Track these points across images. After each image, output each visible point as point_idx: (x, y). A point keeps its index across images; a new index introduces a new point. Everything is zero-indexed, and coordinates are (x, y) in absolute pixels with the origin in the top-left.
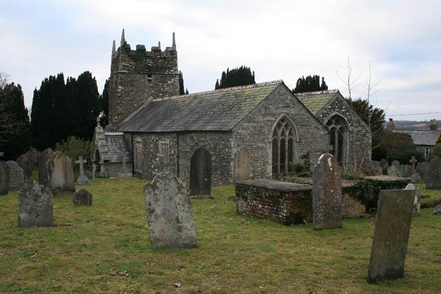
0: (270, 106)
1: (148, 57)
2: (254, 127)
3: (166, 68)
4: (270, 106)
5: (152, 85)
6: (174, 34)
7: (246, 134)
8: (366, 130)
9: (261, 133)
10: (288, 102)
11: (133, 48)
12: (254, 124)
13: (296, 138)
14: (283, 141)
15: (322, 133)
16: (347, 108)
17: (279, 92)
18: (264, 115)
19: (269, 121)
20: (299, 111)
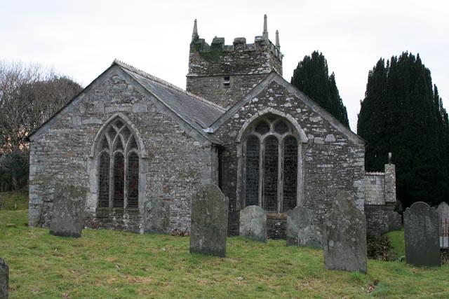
0: (95, 103)
1: (225, 53)
2: (67, 135)
3: (250, 67)
4: (95, 103)
5: (229, 90)
6: (196, 21)
7: (52, 145)
8: (347, 141)
9: (77, 143)
10: (128, 93)
11: (209, 42)
12: (66, 131)
13: (142, 153)
14: (119, 158)
15: (196, 143)
16: (296, 99)
17: (111, 79)
18: (84, 116)
19: (92, 125)
20: (149, 107)
